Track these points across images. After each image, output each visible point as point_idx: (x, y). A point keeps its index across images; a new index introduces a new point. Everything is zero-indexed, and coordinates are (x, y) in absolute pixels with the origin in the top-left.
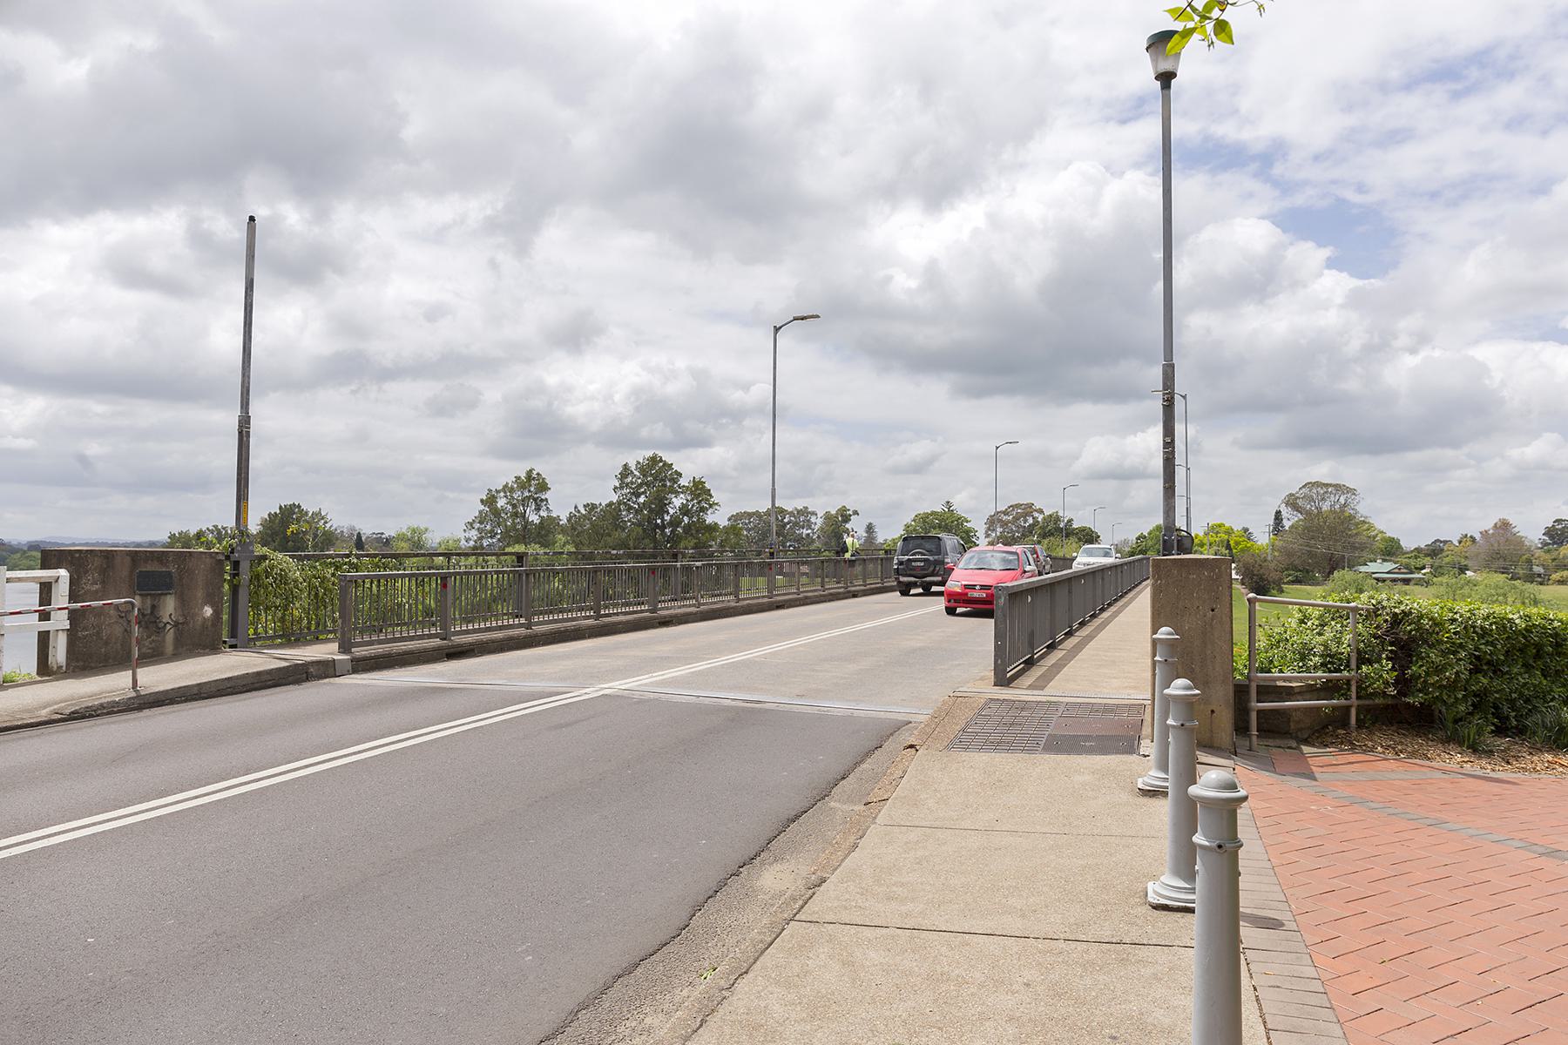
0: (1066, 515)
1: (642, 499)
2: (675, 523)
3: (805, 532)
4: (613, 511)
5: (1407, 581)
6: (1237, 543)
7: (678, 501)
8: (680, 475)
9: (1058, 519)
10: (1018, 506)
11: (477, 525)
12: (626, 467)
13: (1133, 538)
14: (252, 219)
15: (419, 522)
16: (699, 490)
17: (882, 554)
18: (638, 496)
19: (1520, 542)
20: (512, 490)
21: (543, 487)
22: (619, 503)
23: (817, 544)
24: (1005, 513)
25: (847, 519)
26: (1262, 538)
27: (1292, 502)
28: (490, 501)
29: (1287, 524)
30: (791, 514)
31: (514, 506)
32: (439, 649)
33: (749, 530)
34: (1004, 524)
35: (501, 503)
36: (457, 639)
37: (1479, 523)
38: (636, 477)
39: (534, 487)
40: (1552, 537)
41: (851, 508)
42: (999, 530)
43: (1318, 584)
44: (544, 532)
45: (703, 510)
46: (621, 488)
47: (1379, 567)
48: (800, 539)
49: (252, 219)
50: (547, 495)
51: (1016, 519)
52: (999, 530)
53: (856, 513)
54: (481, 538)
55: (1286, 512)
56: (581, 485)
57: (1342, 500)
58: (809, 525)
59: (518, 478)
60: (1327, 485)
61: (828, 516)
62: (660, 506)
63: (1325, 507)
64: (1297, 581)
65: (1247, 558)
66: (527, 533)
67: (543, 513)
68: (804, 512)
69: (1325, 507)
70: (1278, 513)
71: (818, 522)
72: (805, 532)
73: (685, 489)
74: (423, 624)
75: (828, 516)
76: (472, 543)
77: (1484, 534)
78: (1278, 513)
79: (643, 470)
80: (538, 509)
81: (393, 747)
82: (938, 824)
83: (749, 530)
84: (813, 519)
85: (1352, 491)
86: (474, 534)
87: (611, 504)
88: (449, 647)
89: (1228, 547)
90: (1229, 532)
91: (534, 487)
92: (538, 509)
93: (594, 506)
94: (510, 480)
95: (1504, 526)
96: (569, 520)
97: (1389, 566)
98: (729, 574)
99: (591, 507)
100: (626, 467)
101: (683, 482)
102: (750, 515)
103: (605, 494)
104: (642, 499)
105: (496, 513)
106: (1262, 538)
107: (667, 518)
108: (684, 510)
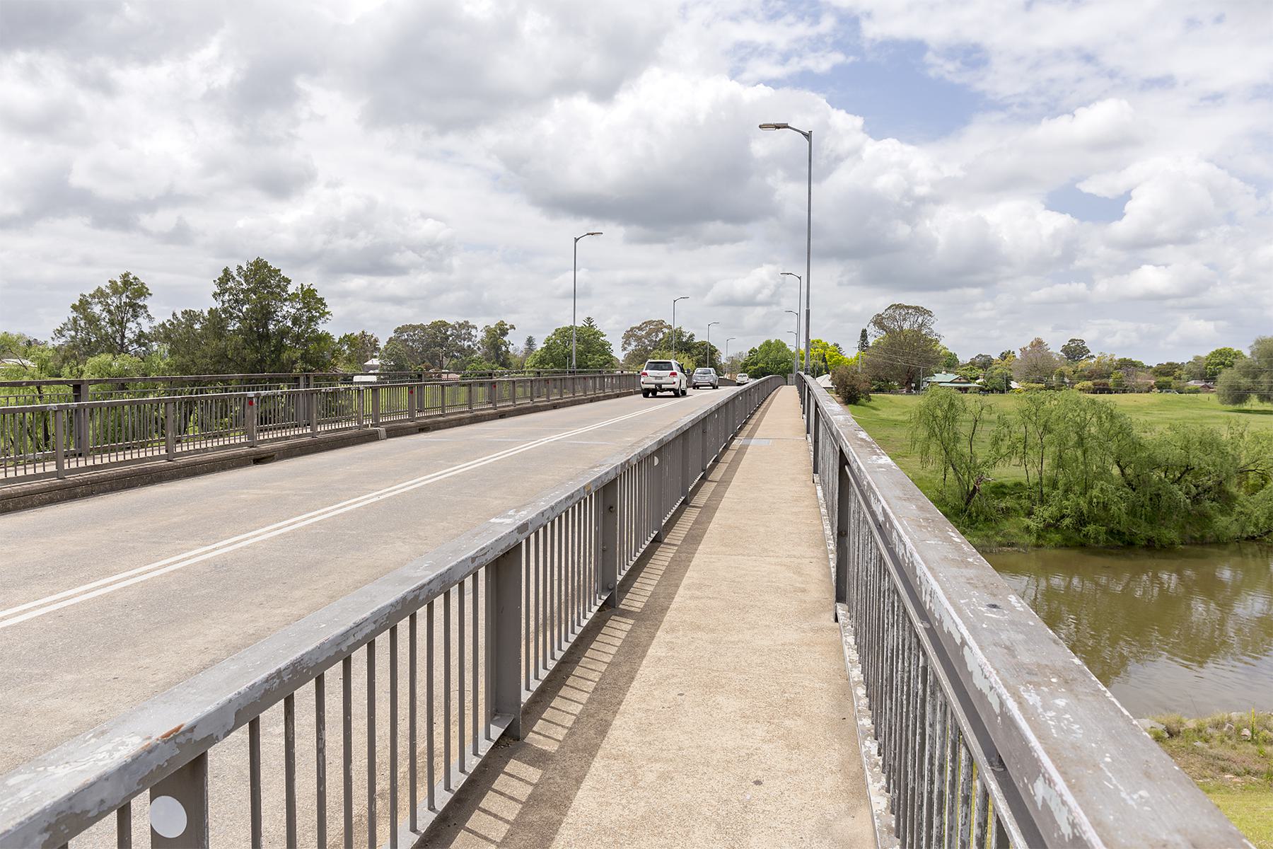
0: (687, 330)
3: (466, 344)
4: (216, 322)
5: (966, 390)
6: (831, 357)
7: (288, 309)
8: (288, 281)
9: (681, 334)
10: (650, 322)
12: (226, 271)
13: (746, 351)
16: (310, 298)
19: (1048, 357)
21: (142, 291)
24: (640, 329)
25: (504, 333)
26: (851, 352)
27: (879, 322)
28: (82, 306)
29: (871, 341)
30: (453, 327)
32: (247, 454)
33: (414, 341)
34: (639, 339)
36: (263, 447)
37: (1017, 343)
40: (1067, 353)
42: (634, 344)
43: (897, 393)
45: (311, 319)
47: (943, 377)
48: (461, 350)
50: (147, 302)
51: (649, 334)
52: (634, 344)
53: (512, 327)
55: (872, 330)
56: (184, 289)
57: (920, 320)
58: (469, 337)
59: (113, 283)
60: (908, 307)
62: (266, 314)
63: (906, 326)
64: (880, 390)
65: (840, 369)
68: (465, 325)
69: (906, 326)
70: (864, 331)
71: (479, 335)
72: (466, 344)
74: (115, 437)
75: (488, 330)
77: (1023, 350)
78: (864, 331)
81: (239, 545)
82: (207, 658)
83: (414, 341)
84: (473, 332)
85: (929, 313)
88: (257, 453)
89: (824, 360)
90: (825, 347)
95: (1038, 344)
97: (951, 377)
98: (569, 383)
100: (226, 271)
101: (291, 289)
102: (415, 328)
103: (205, 303)
105: (92, 321)
106: (851, 352)
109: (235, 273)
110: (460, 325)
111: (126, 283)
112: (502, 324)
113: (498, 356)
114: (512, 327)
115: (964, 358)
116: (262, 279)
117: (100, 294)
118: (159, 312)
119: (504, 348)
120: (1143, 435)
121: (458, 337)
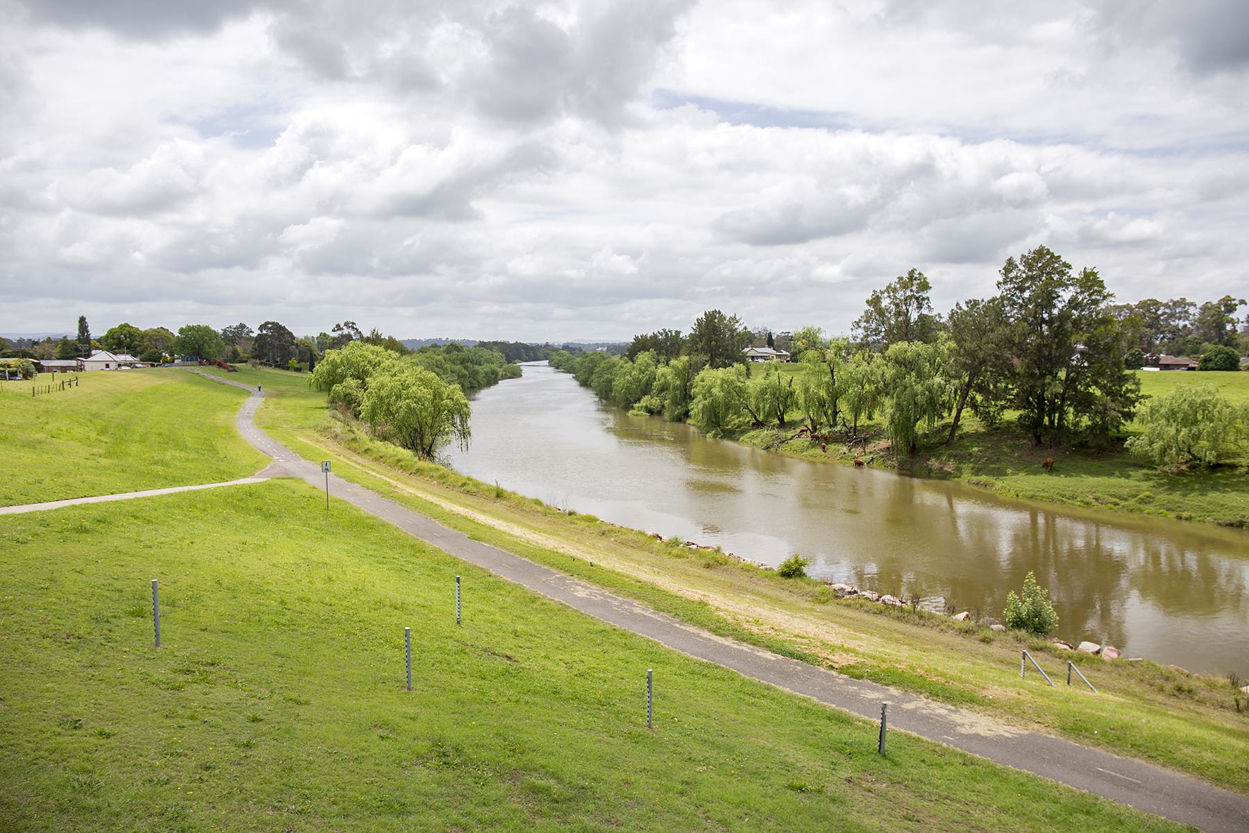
1: (1027, 294)
2: (1064, 316)
3: (1181, 323)
4: (995, 309)
7: (1066, 295)
8: (1069, 267)
11: (863, 324)
14: (82, 320)
15: (815, 325)
16: (1090, 281)
17: (428, 440)
18: (1022, 290)
20: (895, 290)
21: (925, 286)
22: (1002, 298)
23: (1195, 335)
25: (1231, 308)
28: (875, 301)
30: (1166, 306)
31: (897, 305)
35: (885, 302)
38: (1021, 270)
39: (916, 284)
41: (1236, 296)
44: (925, 330)
45: (1096, 302)
46: (1005, 282)
48: (1175, 331)
49: (82, 320)
53: (1243, 302)
54: (867, 336)
59: (900, 279)
61: (1205, 309)
62: (1048, 299)
66: (905, 331)
67: (925, 311)
72: (1181, 323)
73: (1074, 282)
76: (859, 341)
79: (1029, 263)
80: (920, 307)
86: (860, 333)
87: (993, 300)
91: (916, 284)
92: (920, 307)
93: (976, 303)
94: (893, 281)
96: (951, 317)
99: (973, 304)
104: (1027, 294)
105: (881, 312)
107: (1055, 312)
108: (1074, 304)
109: (1018, 262)
110: (1175, 303)
111: (911, 278)
112: (1228, 299)
113: (1220, 336)
114: (1243, 302)
115: (686, 332)
116: (1044, 264)
117: (890, 289)
118: (941, 307)
119: (1229, 327)
120: (18, 455)
121: (1172, 316)
